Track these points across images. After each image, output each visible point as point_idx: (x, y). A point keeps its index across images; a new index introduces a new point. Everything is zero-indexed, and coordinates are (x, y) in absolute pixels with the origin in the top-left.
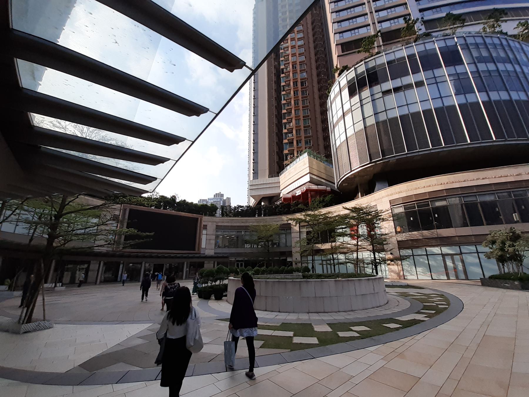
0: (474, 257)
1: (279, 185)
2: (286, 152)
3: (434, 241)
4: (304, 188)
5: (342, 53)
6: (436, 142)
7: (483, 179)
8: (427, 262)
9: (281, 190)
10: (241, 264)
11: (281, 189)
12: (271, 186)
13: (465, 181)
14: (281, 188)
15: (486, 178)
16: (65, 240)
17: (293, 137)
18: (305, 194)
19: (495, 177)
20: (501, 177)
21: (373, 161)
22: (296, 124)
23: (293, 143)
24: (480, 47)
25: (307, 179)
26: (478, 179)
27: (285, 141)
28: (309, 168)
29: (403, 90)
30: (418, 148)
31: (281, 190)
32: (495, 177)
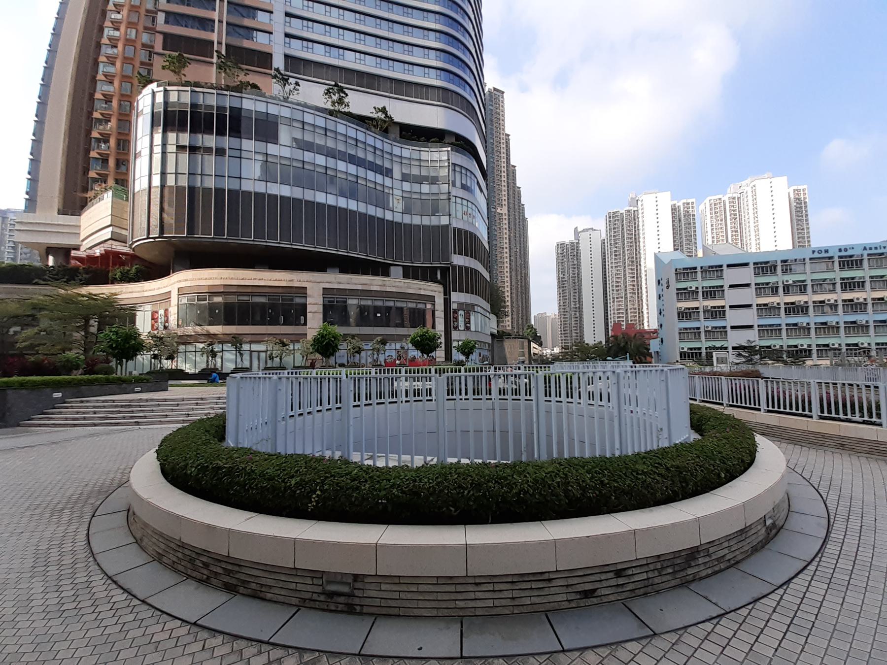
0: (233, 354)
2: (92, 174)
3: (203, 337)
5: (163, 49)
6: (219, 231)
7: (260, 280)
8: (194, 358)
9: (83, 241)
10: (786, 409)
11: (82, 238)
12: (47, 230)
13: (243, 279)
14: (83, 236)
15: (262, 279)
16: (208, 578)
17: (109, 152)
19: (270, 280)
20: (276, 280)
21: (165, 235)
22: (119, 127)
23: (108, 163)
24: (328, 134)
25: (107, 234)
26: (255, 279)
27: (93, 154)
28: (112, 218)
29: (202, 153)
30: (200, 233)
31: (83, 241)
32: (270, 280)
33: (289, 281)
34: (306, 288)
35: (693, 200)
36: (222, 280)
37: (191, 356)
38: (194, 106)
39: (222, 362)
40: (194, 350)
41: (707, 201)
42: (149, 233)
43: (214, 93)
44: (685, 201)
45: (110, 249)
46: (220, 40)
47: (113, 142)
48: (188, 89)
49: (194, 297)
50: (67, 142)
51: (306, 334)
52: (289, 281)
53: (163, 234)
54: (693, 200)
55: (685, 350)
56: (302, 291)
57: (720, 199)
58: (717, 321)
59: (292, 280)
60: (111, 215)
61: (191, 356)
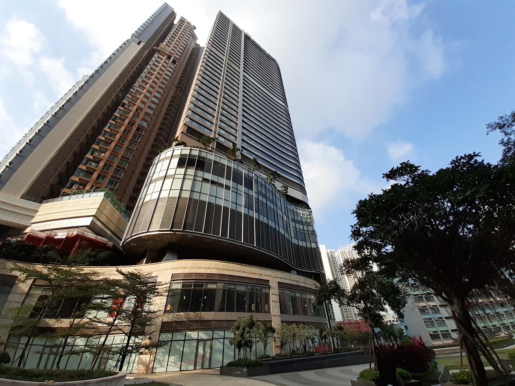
1: (32, 215)
4: (75, 232)
6: (224, 234)
7: (243, 272)
8: (182, 349)
11: (32, 222)
13: (232, 271)
18: (70, 241)
21: (173, 229)
25: (87, 222)
32: (249, 273)
33: (260, 275)
34: (269, 281)
35: (333, 250)
36: (218, 270)
37: (178, 347)
38: (199, 157)
39: (211, 353)
40: (183, 339)
41: (339, 251)
42: (172, 228)
43: (213, 155)
44: (330, 250)
45: (81, 234)
46: (215, 133)
47: (102, 164)
48: (198, 149)
49: (191, 284)
50: (56, 154)
51: (271, 321)
52: (260, 275)
53: (172, 228)
54: (333, 250)
55: (432, 333)
56: (265, 283)
57: (344, 251)
58: (426, 315)
59: (261, 275)
60: (98, 208)
61: (178, 347)
